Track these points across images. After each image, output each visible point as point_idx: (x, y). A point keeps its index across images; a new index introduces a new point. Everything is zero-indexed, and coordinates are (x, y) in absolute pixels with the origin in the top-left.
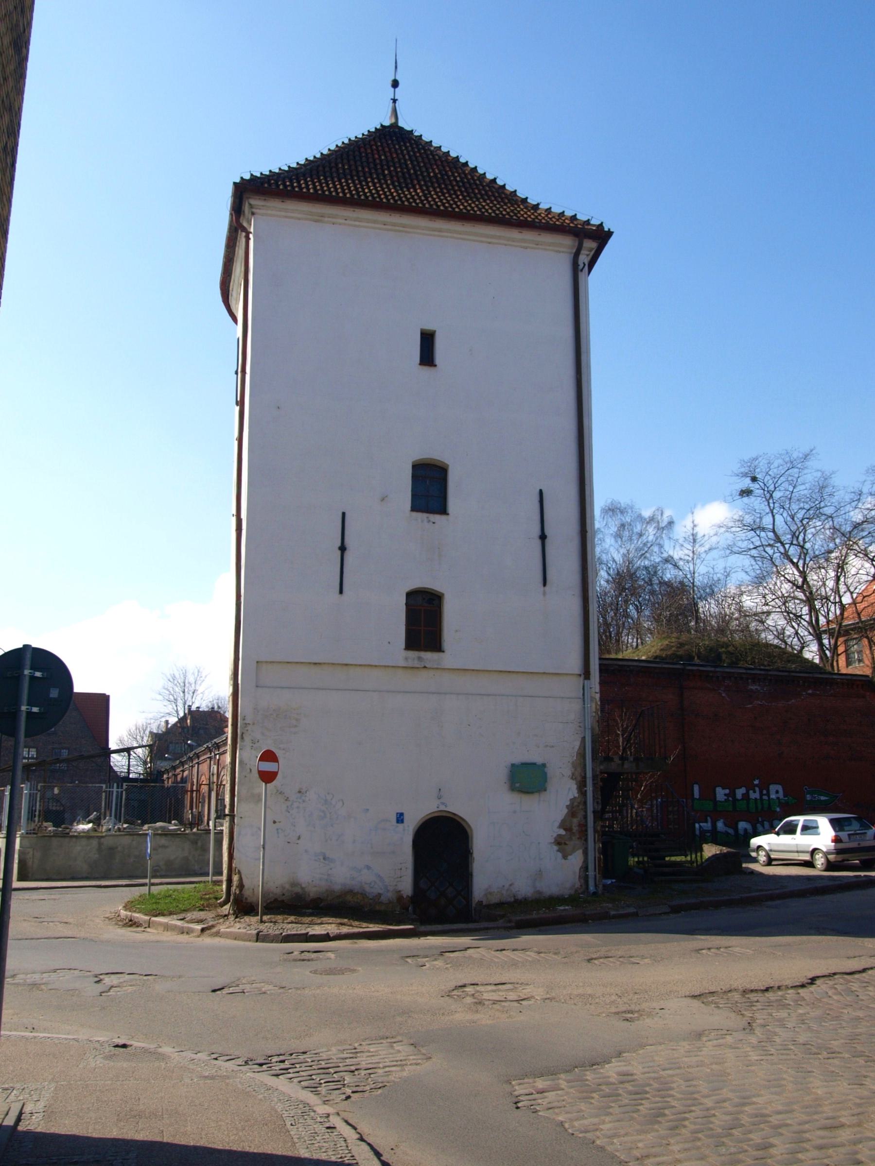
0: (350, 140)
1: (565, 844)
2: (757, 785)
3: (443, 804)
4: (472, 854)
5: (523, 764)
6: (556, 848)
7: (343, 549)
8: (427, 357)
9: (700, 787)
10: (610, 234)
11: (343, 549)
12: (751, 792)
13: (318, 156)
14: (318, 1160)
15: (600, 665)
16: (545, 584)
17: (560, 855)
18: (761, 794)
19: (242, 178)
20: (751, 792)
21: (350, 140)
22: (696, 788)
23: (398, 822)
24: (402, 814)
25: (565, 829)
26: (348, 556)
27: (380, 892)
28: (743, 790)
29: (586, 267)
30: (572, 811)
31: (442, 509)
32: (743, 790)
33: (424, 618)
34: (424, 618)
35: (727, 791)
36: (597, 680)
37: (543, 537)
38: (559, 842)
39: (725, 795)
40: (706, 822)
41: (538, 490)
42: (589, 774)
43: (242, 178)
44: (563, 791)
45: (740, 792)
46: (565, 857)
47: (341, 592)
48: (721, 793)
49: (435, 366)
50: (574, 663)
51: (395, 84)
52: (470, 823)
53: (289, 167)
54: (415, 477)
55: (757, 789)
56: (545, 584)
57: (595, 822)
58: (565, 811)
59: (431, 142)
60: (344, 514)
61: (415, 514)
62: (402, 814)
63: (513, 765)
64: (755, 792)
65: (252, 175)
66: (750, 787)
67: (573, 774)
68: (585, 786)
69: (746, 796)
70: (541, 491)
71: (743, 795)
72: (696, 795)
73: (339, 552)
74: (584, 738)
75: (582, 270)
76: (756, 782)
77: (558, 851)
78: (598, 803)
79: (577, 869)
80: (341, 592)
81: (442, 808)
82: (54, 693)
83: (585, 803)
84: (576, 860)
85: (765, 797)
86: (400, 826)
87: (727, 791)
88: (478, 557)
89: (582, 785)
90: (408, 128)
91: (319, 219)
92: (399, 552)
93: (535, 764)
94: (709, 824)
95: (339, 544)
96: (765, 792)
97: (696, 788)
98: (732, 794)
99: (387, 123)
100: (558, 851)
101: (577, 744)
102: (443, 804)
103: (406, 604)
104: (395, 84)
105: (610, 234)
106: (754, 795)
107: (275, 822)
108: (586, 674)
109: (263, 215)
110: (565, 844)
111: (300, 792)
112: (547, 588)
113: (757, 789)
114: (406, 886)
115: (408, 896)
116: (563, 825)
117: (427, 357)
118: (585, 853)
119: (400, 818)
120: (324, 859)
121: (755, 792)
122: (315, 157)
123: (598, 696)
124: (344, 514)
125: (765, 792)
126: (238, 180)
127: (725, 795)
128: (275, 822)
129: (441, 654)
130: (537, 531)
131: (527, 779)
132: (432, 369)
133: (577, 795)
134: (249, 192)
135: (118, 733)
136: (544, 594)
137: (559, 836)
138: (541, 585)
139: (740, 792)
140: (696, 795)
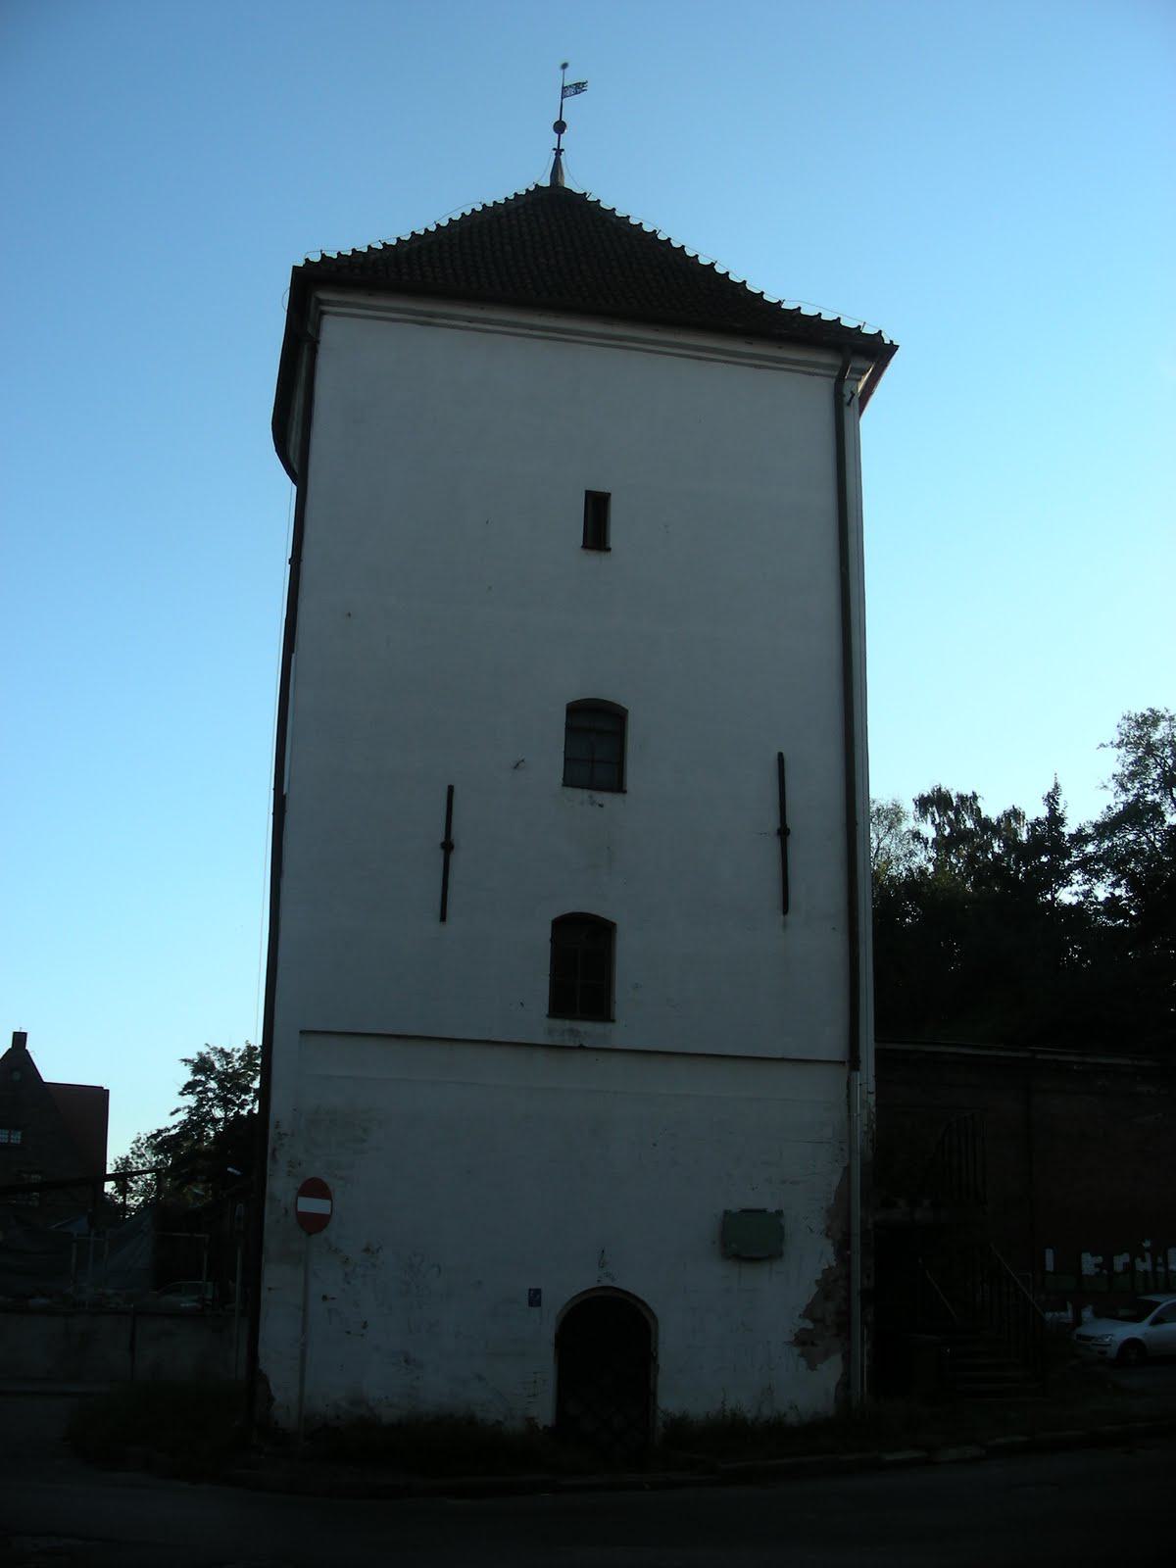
0: (484, 206)
1: (813, 1344)
2: (1148, 1250)
3: (608, 1275)
4: (655, 1359)
5: (744, 1211)
6: (797, 1351)
7: (448, 847)
8: (596, 536)
9: (1054, 1252)
10: (892, 349)
11: (448, 847)
12: (1138, 1261)
13: (433, 228)
14: (1119, 1349)
15: (877, 1051)
16: (785, 910)
17: (803, 1362)
18: (1155, 1264)
19: (307, 260)
20: (1138, 1261)
21: (484, 206)
22: (1049, 1255)
23: (531, 1304)
24: (538, 1292)
25: (814, 1321)
26: (456, 858)
27: (501, 1419)
28: (1125, 1258)
29: (856, 400)
30: (827, 1286)
31: (616, 784)
32: (1125, 1258)
33: (582, 964)
34: (582, 964)
35: (1100, 1259)
36: (872, 1072)
37: (783, 832)
38: (803, 1341)
39: (1097, 1265)
40: (1065, 1309)
41: (773, 758)
42: (856, 1229)
43: (307, 260)
44: (809, 1257)
45: (1120, 1262)
46: (812, 1366)
47: (443, 918)
48: (1089, 1263)
49: (609, 549)
50: (830, 1042)
51: (560, 127)
52: (651, 1305)
53: (384, 244)
54: (571, 730)
55: (1147, 1255)
56: (785, 910)
57: (863, 1310)
58: (815, 1289)
59: (614, 209)
60: (451, 789)
61: (569, 791)
62: (538, 1292)
63: (726, 1213)
64: (1144, 1260)
65: (323, 255)
66: (1137, 1252)
67: (829, 1228)
68: (848, 1248)
69: (1130, 1268)
70: (781, 757)
71: (1125, 1264)
72: (1050, 1265)
73: (441, 853)
74: (847, 1170)
75: (849, 404)
76: (1147, 1244)
77: (802, 1355)
78: (868, 1277)
79: (832, 1385)
80: (443, 918)
81: (607, 1282)
82: (17, 1076)
83: (848, 1277)
84: (831, 1371)
85: (1160, 1269)
86: (535, 1310)
87: (1100, 1259)
88: (673, 865)
89: (843, 1247)
90: (579, 191)
91: (427, 321)
92: (542, 851)
93: (764, 1211)
94: (1070, 1313)
95: (441, 838)
96: (1160, 1260)
97: (1049, 1255)
98: (1108, 1264)
99: (546, 182)
100: (802, 1355)
101: (836, 1179)
102: (608, 1275)
103: (552, 940)
104: (560, 127)
105: (892, 349)
106: (1143, 1266)
107: (325, 1298)
108: (853, 1062)
109: (336, 314)
110: (813, 1344)
111: (367, 1250)
112: (790, 916)
113: (1147, 1255)
114: (544, 1412)
115: (545, 1427)
116: (808, 1313)
117: (596, 536)
118: (847, 1358)
119: (535, 1298)
120: (406, 1361)
121: (1144, 1260)
122: (426, 230)
123: (872, 1099)
124: (451, 789)
125: (1160, 1260)
126: (301, 263)
127: (1097, 1265)
128: (325, 1298)
129: (610, 1026)
130: (774, 824)
131: (749, 1239)
132: (604, 556)
133: (834, 1264)
134: (317, 286)
135: (119, 1146)
136: (785, 925)
137: (803, 1330)
138: (780, 912)
139: (1120, 1262)
140: (1050, 1265)
